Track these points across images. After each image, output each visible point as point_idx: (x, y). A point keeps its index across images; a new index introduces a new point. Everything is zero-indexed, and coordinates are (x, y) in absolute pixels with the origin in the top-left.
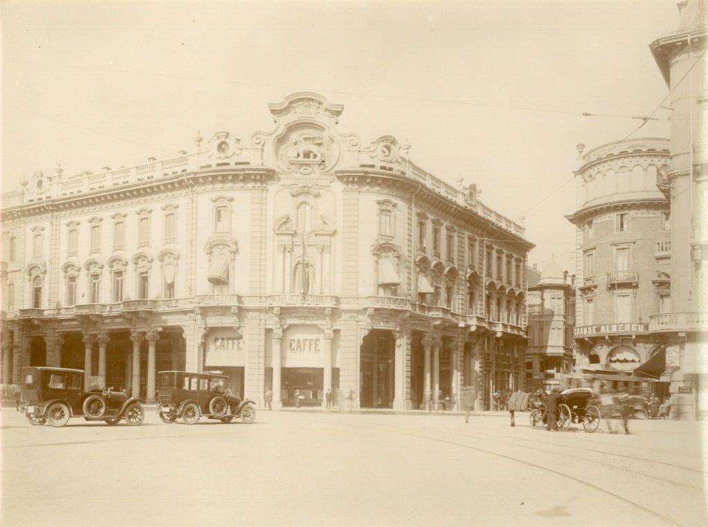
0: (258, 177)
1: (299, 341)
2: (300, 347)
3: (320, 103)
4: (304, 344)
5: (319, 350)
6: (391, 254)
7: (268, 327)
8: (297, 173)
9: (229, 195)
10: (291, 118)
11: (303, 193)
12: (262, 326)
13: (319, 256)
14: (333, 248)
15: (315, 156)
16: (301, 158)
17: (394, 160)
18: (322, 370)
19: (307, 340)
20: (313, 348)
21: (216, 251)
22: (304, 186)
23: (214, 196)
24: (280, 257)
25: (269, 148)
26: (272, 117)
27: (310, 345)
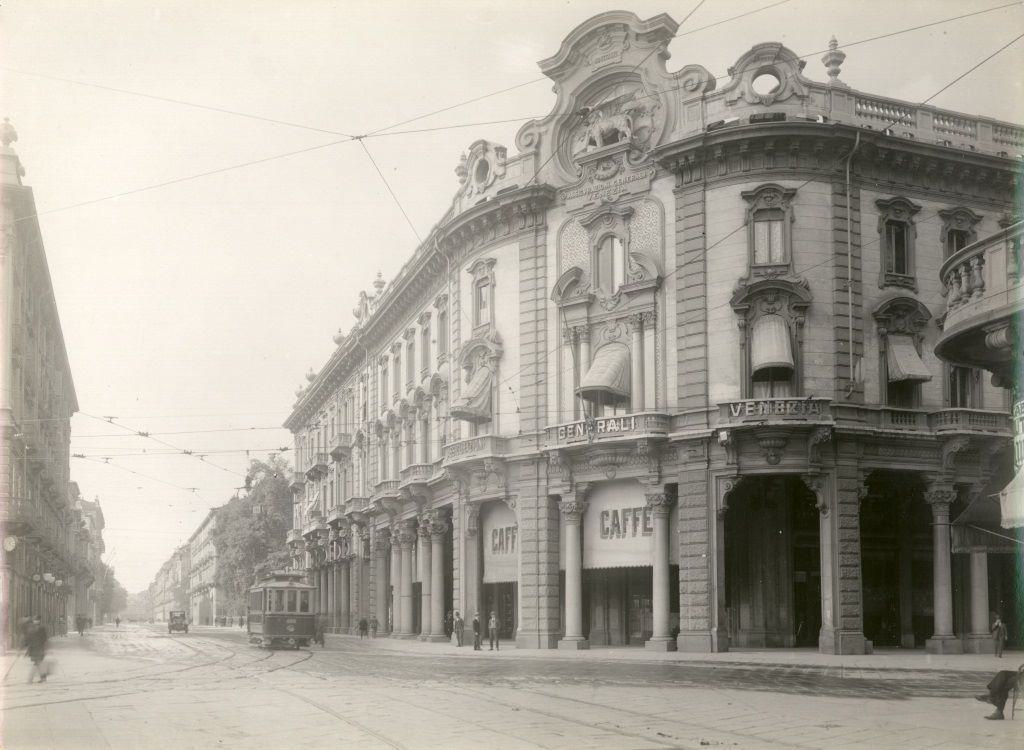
1: (615, 513)
2: (617, 525)
4: (625, 520)
5: (651, 530)
6: (784, 306)
7: (553, 492)
8: (591, 181)
9: (788, 184)
10: (584, 74)
11: (608, 217)
12: (542, 492)
13: (635, 336)
14: (660, 317)
16: (599, 147)
17: (787, 94)
18: (650, 569)
19: (629, 510)
20: (640, 528)
21: (477, 361)
24: (568, 352)
27: (636, 520)
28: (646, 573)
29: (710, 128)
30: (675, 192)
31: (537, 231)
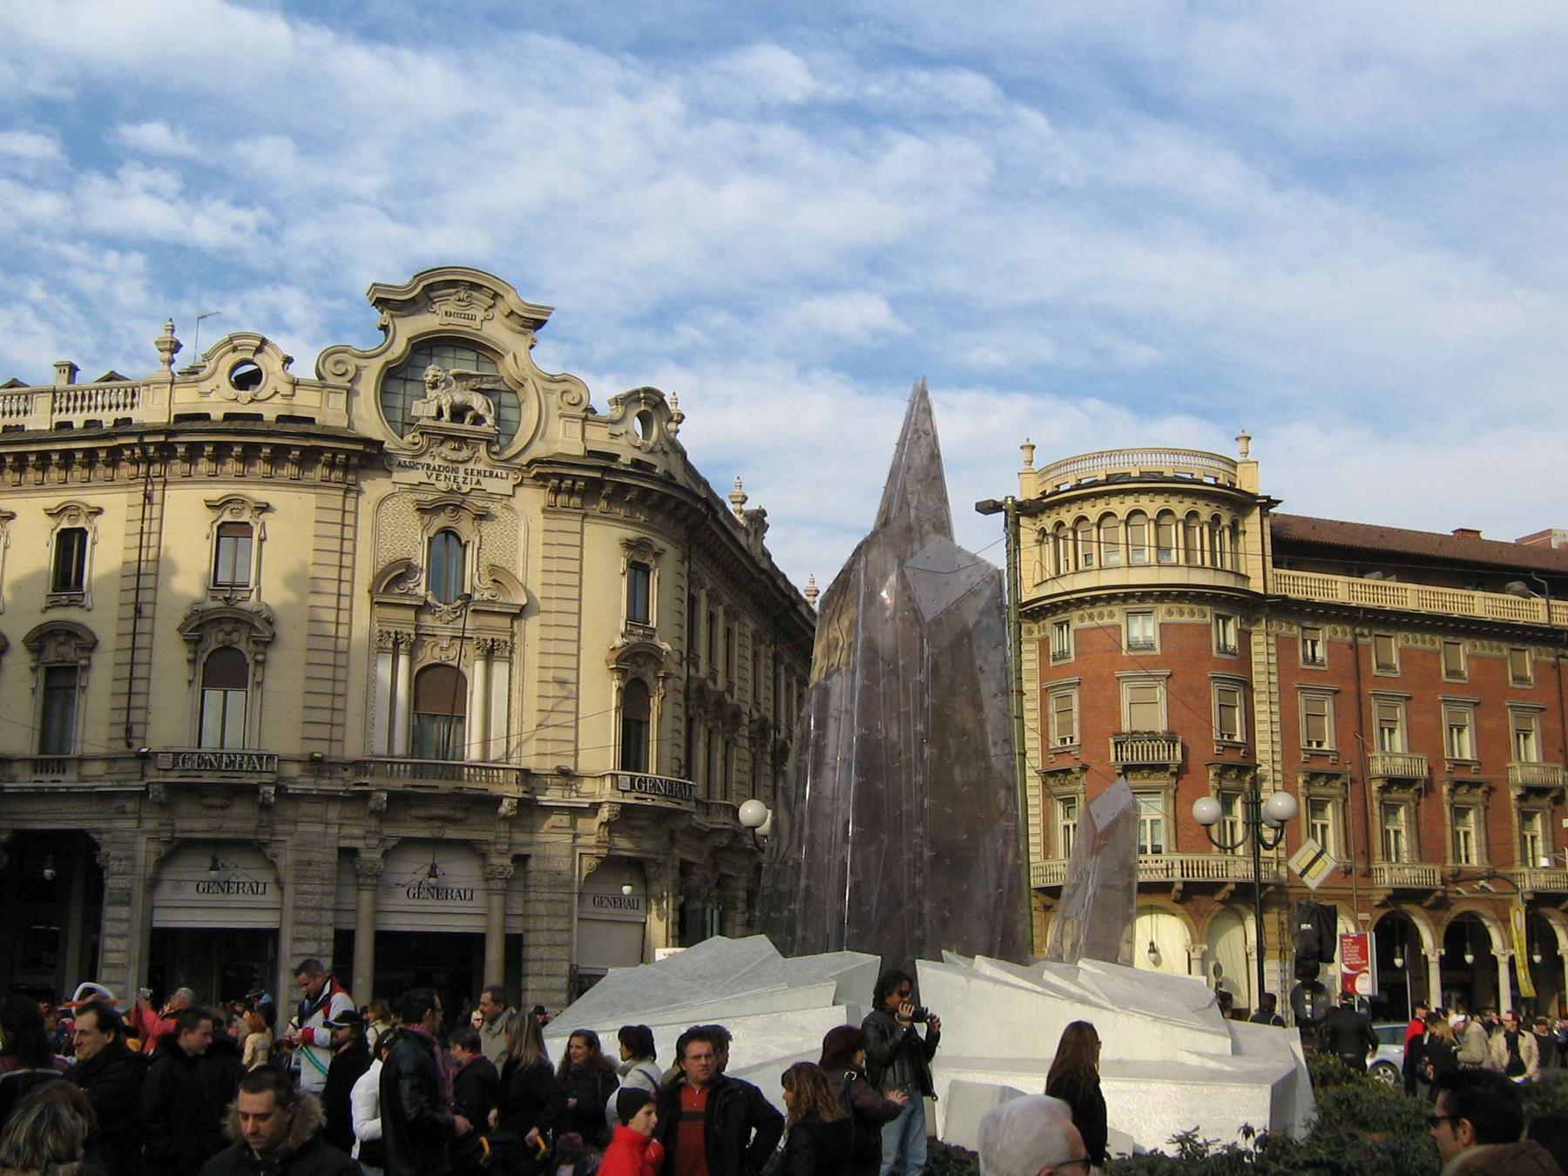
0: (354, 461)
3: (496, 296)
7: (344, 843)
9: (259, 494)
13: (479, 666)
15: (478, 419)
16: (445, 421)
22: (451, 491)
23: (217, 492)
25: (368, 387)
26: (378, 317)
28: (472, 944)
29: (180, 418)
30: (544, 511)
31: (347, 491)
